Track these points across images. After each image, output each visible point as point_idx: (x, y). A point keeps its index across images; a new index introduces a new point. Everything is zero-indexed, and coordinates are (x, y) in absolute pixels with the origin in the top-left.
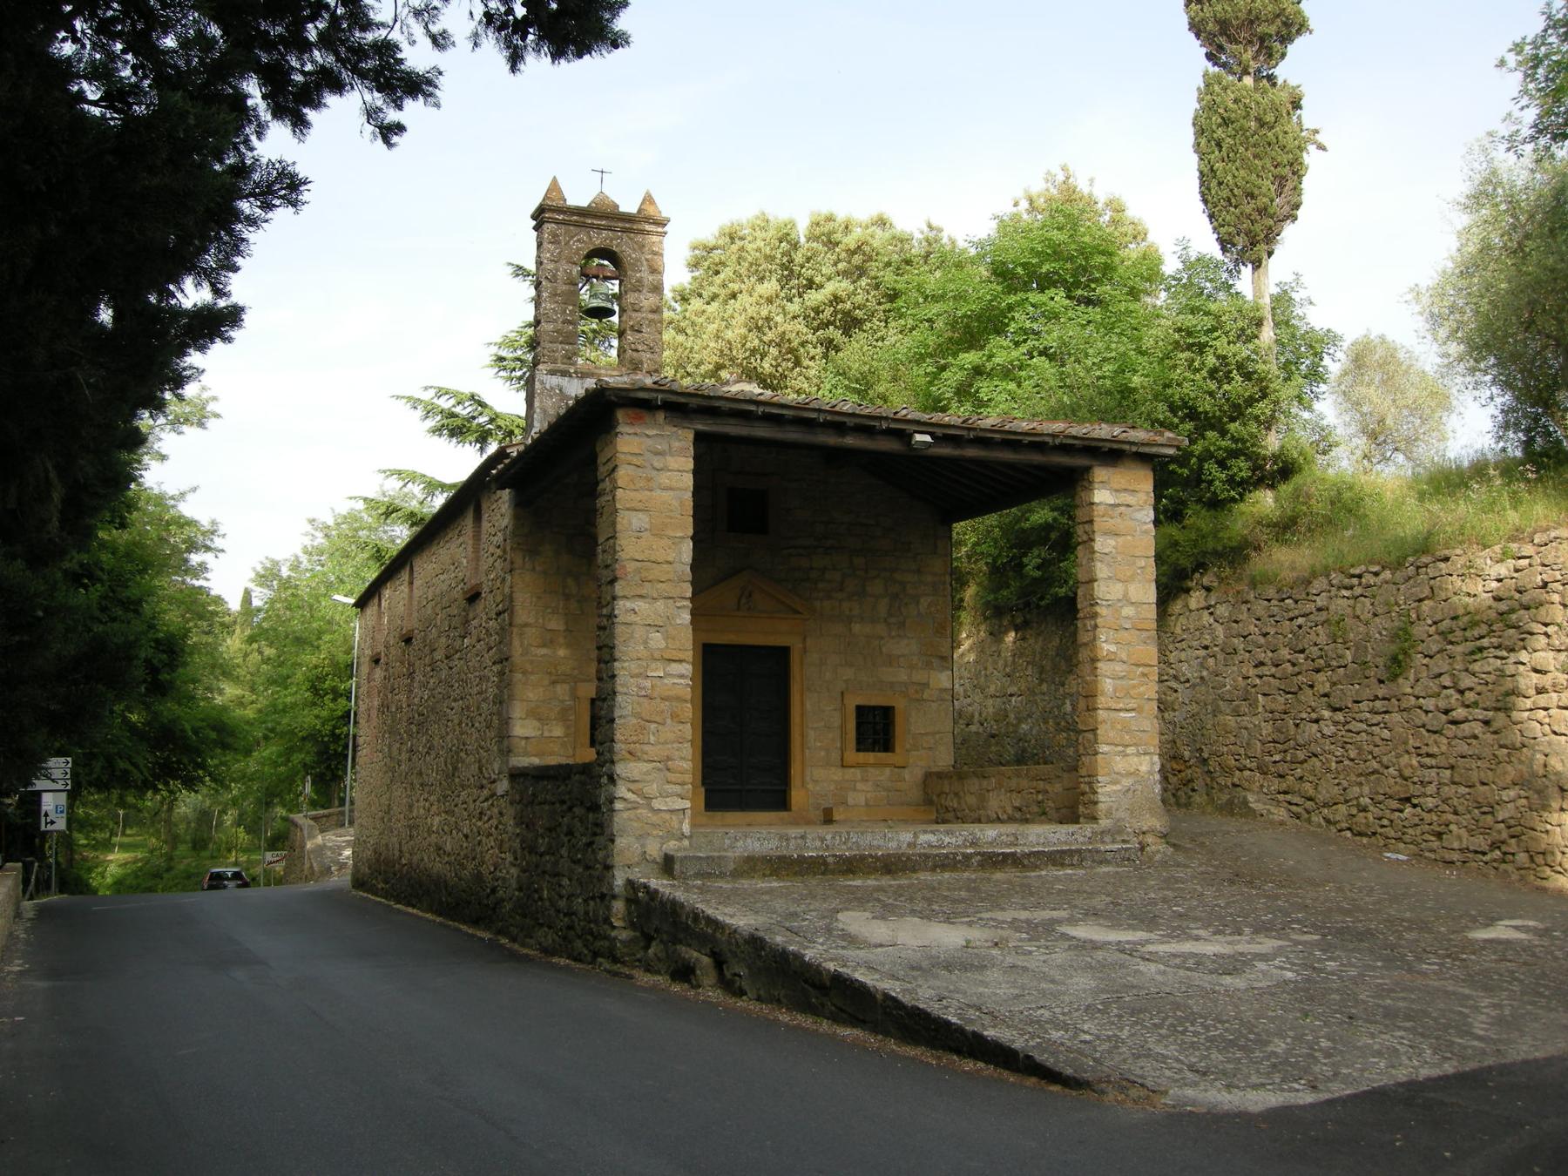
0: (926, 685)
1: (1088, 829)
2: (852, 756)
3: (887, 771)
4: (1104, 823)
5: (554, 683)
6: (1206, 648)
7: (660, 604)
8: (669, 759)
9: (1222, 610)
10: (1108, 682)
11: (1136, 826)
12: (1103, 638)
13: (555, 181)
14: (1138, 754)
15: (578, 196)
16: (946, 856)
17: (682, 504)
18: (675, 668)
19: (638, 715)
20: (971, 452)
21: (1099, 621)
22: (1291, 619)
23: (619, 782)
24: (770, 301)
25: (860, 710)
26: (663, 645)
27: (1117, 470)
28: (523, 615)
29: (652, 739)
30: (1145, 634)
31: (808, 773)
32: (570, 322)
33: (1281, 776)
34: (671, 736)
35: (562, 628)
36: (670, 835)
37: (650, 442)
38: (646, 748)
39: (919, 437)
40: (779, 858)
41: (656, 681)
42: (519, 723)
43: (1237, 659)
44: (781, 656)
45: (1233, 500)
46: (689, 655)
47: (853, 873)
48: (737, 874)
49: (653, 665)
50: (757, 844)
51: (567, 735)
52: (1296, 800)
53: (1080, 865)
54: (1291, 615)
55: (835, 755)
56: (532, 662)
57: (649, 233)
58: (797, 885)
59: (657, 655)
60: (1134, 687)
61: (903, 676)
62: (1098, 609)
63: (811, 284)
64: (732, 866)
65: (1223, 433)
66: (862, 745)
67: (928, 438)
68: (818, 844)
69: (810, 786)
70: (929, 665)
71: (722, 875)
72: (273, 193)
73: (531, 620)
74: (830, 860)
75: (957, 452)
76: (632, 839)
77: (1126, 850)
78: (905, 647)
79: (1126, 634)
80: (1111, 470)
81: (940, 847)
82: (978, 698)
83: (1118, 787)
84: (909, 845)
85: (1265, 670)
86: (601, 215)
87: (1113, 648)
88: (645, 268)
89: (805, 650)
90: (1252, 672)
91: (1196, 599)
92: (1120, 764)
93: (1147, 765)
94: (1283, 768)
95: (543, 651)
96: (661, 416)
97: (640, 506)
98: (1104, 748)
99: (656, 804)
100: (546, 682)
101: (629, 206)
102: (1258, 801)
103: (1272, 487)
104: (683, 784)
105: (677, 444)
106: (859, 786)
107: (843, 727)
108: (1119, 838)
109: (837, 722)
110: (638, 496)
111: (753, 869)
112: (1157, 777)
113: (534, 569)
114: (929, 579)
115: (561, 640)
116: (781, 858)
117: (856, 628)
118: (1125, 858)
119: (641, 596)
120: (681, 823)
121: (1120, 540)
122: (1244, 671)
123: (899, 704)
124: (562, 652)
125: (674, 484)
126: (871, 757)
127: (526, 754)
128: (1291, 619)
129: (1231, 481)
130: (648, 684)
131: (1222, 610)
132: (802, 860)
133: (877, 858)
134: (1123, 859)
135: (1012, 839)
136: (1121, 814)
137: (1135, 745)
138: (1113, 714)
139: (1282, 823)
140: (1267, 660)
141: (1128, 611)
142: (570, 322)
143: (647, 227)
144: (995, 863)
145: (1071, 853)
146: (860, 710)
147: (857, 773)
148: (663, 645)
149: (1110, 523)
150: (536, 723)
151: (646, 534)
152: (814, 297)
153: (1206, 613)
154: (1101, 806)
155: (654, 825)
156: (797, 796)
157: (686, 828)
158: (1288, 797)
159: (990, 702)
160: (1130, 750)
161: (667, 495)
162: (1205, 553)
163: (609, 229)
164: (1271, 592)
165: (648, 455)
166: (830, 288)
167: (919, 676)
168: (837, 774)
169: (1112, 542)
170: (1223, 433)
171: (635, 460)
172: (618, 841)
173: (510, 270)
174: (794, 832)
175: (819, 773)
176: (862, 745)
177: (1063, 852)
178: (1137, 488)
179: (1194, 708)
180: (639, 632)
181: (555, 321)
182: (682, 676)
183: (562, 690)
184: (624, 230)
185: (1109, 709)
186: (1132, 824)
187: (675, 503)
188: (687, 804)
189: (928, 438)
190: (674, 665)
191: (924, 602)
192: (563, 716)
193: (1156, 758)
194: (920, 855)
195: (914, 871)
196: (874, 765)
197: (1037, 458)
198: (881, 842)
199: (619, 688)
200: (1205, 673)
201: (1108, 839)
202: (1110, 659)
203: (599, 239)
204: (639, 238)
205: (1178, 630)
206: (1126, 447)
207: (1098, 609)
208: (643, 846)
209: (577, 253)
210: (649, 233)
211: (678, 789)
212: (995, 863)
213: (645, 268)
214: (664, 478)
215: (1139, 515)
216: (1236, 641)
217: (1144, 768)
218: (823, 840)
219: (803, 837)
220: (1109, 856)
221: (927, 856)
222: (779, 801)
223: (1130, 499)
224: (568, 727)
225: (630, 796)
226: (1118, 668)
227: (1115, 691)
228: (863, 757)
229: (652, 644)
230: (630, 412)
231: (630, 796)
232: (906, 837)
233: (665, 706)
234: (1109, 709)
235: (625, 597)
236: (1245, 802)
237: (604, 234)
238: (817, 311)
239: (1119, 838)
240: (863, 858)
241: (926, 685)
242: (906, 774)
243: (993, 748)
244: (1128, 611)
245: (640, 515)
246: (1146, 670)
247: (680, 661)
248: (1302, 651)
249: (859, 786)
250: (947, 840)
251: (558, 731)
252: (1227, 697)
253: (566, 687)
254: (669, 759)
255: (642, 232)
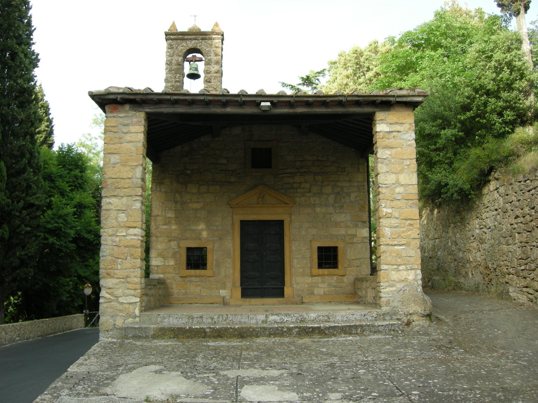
0: (355, 236)
1: (375, 312)
2: (316, 271)
3: (335, 278)
4: (385, 309)
5: (170, 241)
6: (496, 210)
7: (125, 200)
8: (128, 277)
9: (502, 190)
10: (386, 230)
11: (405, 311)
12: (383, 205)
13: (174, 23)
14: (407, 270)
15: (183, 28)
16: (277, 329)
17: (137, 149)
18: (132, 231)
19: (112, 255)
20: (300, 110)
21: (381, 196)
22: (529, 191)
23: (102, 289)
24: (348, 77)
25: (320, 249)
26: (126, 219)
27: (390, 112)
28: (155, 212)
29: (119, 267)
30: (411, 202)
31: (294, 279)
32: (178, 82)
33: (525, 278)
34: (129, 265)
35: (174, 216)
36: (129, 315)
37: (121, 120)
38: (116, 271)
39: (263, 104)
40: (179, 329)
41: (123, 238)
42: (154, 259)
43: (508, 214)
44: (280, 224)
45: (509, 133)
46: (139, 224)
47: (221, 337)
48: (154, 337)
49: (120, 230)
50: (175, 321)
51: (176, 264)
52: (531, 291)
53: (362, 334)
54: (529, 189)
55: (308, 271)
56: (160, 232)
57: (214, 39)
58: (191, 343)
59: (122, 225)
60: (404, 232)
61: (343, 232)
62: (380, 190)
63: (369, 69)
64: (152, 333)
65: (498, 98)
66: (321, 266)
67: (268, 104)
68: (210, 321)
69: (295, 286)
70: (356, 226)
71: (146, 337)
72: (516, 123)
73: (160, 213)
74: (208, 330)
75: (291, 111)
76: (108, 317)
77: (392, 325)
78: (343, 217)
79: (398, 202)
80: (387, 113)
81: (281, 323)
82: (427, 240)
83: (394, 289)
84: (263, 322)
85: (519, 220)
86: (196, 34)
87: (389, 211)
88: (212, 54)
89: (291, 221)
90: (514, 221)
91: (492, 185)
92: (394, 276)
93: (414, 276)
94: (525, 273)
95: (165, 227)
96: (127, 107)
97: (116, 151)
98: (384, 267)
99: (121, 300)
100: (166, 241)
101: (205, 28)
102: (514, 291)
103: (531, 124)
104: (135, 290)
105: (135, 120)
106: (320, 285)
107: (311, 257)
108: (394, 317)
109: (308, 255)
110: (114, 147)
111: (164, 334)
112: (420, 282)
113: (160, 191)
114: (356, 184)
115: (173, 222)
116: (180, 329)
117: (318, 209)
118: (391, 330)
119: (115, 196)
120: (135, 309)
121: (394, 151)
122: (510, 221)
123: (340, 245)
124: (174, 227)
125: (133, 140)
126: (326, 271)
127: (157, 273)
128: (529, 191)
129: (505, 123)
130: (117, 239)
131: (502, 190)
132: (191, 330)
133: (235, 329)
134: (390, 330)
135: (326, 318)
136: (396, 304)
137: (405, 264)
138: (392, 248)
139: (522, 305)
140: (519, 215)
141: (399, 190)
142: (178, 82)
143: (214, 36)
144: (307, 333)
145: (356, 327)
146: (320, 249)
147: (319, 278)
148: (126, 219)
149: (387, 142)
150: (162, 260)
151: (119, 165)
152: (370, 74)
153: (496, 192)
154: (383, 299)
155: (121, 311)
156: (287, 290)
157: (137, 312)
158: (528, 290)
159: (431, 242)
160: (401, 268)
161: (129, 145)
162: (493, 161)
163: (196, 39)
164: (521, 178)
165: (121, 126)
166: (375, 69)
167: (351, 231)
168: (309, 280)
169: (388, 152)
170: (498, 98)
171: (114, 130)
172: (101, 318)
173: (280, 84)
174: (196, 314)
175: (300, 279)
176: (321, 266)
177: (350, 326)
178: (404, 121)
179: (492, 241)
180: (113, 214)
181: (171, 82)
182: (135, 235)
183: (173, 244)
184: (203, 39)
185: (388, 245)
186: (402, 310)
187: (134, 149)
188: (138, 300)
189: (268, 104)
190: (131, 230)
191: (353, 195)
192: (174, 255)
193: (419, 272)
194: (261, 328)
195: (257, 336)
196: (328, 275)
197: (340, 110)
198: (246, 320)
199: (102, 242)
200: (496, 223)
201: (387, 318)
202: (388, 216)
203: (191, 44)
204: (210, 42)
205: (486, 202)
206: (392, 99)
207: (380, 190)
208: (115, 321)
209: (181, 51)
210: (214, 39)
211: (132, 292)
212: (307, 333)
213: (212, 54)
214: (128, 137)
215: (405, 137)
216: (507, 205)
217: (411, 277)
218: (212, 319)
219: (201, 317)
220: (381, 329)
221: (265, 329)
222: (279, 292)
223: (398, 128)
224: (176, 261)
225: (107, 296)
226: (394, 222)
227: (392, 234)
228: (321, 271)
229: (120, 219)
230: (111, 106)
231: (107, 296)
232: (262, 317)
233: (126, 250)
234: (388, 245)
235: (106, 197)
236: (508, 292)
237: (193, 42)
238: (370, 80)
239: (394, 317)
240: (226, 329)
241: (355, 236)
242: (345, 279)
243: (431, 264)
244: (399, 190)
245: (116, 156)
246: (411, 222)
247: (135, 227)
248: (533, 208)
249: (320, 285)
250: (286, 319)
251: (172, 263)
252: (504, 235)
253: (175, 242)
254: (128, 277)
255: (210, 39)
